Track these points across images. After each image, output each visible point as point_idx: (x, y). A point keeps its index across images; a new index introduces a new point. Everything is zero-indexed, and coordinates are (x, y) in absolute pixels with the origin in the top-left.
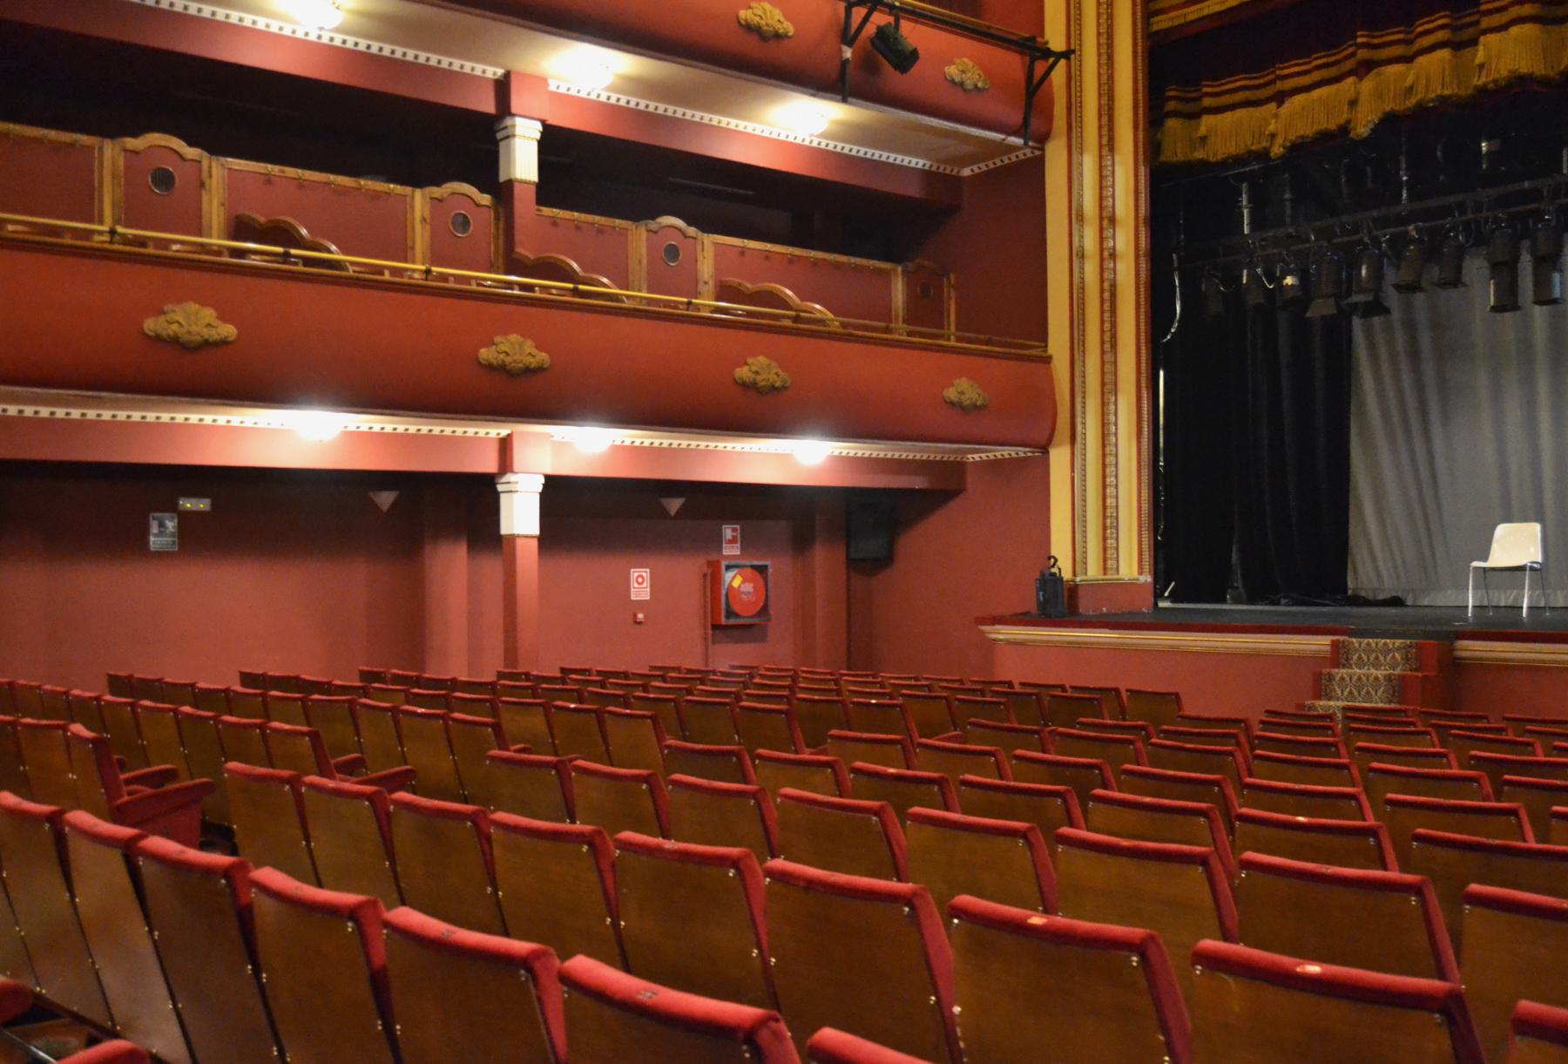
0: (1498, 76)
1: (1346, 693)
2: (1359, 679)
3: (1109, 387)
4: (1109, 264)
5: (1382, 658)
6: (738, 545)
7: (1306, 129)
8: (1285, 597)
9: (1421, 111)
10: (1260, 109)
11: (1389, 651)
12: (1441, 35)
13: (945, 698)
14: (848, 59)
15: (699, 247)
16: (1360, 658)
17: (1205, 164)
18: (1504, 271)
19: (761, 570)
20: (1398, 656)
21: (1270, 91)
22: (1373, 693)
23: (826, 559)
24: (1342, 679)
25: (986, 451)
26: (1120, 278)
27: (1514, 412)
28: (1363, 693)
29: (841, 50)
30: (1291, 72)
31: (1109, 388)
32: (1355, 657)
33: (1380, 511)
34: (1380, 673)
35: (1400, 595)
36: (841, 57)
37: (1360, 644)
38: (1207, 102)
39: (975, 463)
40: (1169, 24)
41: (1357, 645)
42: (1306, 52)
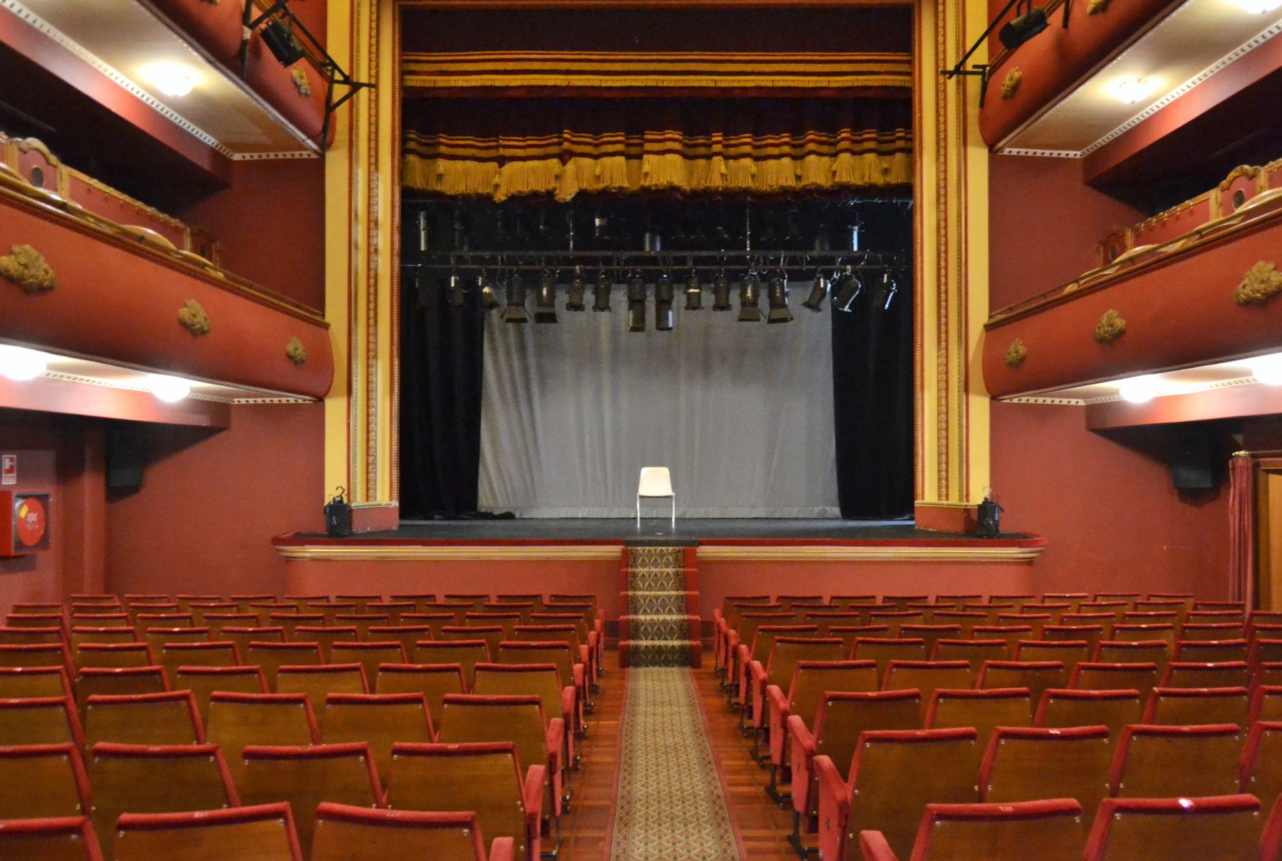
0: (659, 183)
1: (646, 585)
2: (656, 575)
3: (372, 354)
4: (373, 257)
5: (659, 561)
6: (15, 475)
7: (522, 187)
8: (438, 514)
9: (604, 193)
10: (482, 164)
11: (664, 555)
12: (619, 147)
13: (236, 606)
14: (247, 40)
15: (58, 175)
16: (643, 560)
17: (439, 195)
18: (636, 303)
19: (43, 499)
20: (671, 558)
21: (492, 153)
22: (666, 584)
23: (90, 487)
24: (643, 575)
25: (272, 396)
26: (380, 270)
27: (606, 397)
28: (658, 585)
29: (242, 30)
30: (511, 145)
31: (371, 354)
32: (640, 560)
33: (496, 453)
34: (670, 570)
35: (510, 510)
36: (242, 37)
37: (644, 551)
38: (443, 149)
39: (241, 406)
40: (418, 84)
41: (641, 552)
42: (523, 133)
